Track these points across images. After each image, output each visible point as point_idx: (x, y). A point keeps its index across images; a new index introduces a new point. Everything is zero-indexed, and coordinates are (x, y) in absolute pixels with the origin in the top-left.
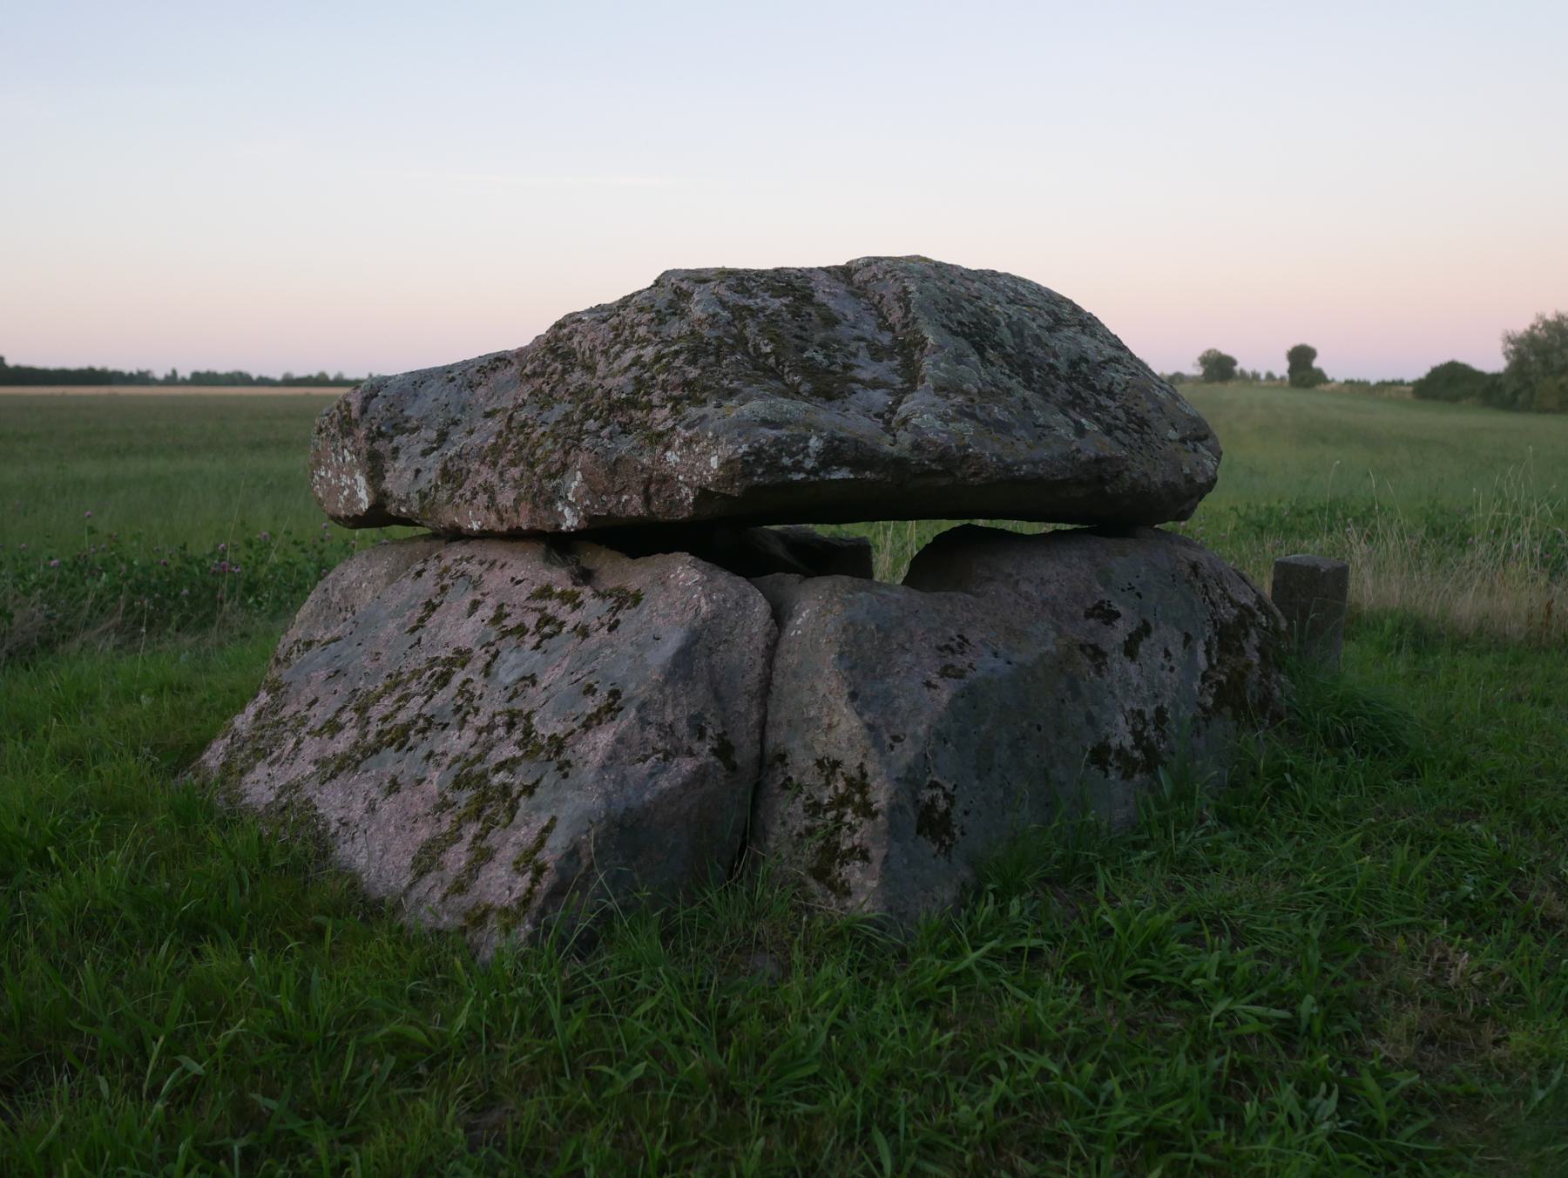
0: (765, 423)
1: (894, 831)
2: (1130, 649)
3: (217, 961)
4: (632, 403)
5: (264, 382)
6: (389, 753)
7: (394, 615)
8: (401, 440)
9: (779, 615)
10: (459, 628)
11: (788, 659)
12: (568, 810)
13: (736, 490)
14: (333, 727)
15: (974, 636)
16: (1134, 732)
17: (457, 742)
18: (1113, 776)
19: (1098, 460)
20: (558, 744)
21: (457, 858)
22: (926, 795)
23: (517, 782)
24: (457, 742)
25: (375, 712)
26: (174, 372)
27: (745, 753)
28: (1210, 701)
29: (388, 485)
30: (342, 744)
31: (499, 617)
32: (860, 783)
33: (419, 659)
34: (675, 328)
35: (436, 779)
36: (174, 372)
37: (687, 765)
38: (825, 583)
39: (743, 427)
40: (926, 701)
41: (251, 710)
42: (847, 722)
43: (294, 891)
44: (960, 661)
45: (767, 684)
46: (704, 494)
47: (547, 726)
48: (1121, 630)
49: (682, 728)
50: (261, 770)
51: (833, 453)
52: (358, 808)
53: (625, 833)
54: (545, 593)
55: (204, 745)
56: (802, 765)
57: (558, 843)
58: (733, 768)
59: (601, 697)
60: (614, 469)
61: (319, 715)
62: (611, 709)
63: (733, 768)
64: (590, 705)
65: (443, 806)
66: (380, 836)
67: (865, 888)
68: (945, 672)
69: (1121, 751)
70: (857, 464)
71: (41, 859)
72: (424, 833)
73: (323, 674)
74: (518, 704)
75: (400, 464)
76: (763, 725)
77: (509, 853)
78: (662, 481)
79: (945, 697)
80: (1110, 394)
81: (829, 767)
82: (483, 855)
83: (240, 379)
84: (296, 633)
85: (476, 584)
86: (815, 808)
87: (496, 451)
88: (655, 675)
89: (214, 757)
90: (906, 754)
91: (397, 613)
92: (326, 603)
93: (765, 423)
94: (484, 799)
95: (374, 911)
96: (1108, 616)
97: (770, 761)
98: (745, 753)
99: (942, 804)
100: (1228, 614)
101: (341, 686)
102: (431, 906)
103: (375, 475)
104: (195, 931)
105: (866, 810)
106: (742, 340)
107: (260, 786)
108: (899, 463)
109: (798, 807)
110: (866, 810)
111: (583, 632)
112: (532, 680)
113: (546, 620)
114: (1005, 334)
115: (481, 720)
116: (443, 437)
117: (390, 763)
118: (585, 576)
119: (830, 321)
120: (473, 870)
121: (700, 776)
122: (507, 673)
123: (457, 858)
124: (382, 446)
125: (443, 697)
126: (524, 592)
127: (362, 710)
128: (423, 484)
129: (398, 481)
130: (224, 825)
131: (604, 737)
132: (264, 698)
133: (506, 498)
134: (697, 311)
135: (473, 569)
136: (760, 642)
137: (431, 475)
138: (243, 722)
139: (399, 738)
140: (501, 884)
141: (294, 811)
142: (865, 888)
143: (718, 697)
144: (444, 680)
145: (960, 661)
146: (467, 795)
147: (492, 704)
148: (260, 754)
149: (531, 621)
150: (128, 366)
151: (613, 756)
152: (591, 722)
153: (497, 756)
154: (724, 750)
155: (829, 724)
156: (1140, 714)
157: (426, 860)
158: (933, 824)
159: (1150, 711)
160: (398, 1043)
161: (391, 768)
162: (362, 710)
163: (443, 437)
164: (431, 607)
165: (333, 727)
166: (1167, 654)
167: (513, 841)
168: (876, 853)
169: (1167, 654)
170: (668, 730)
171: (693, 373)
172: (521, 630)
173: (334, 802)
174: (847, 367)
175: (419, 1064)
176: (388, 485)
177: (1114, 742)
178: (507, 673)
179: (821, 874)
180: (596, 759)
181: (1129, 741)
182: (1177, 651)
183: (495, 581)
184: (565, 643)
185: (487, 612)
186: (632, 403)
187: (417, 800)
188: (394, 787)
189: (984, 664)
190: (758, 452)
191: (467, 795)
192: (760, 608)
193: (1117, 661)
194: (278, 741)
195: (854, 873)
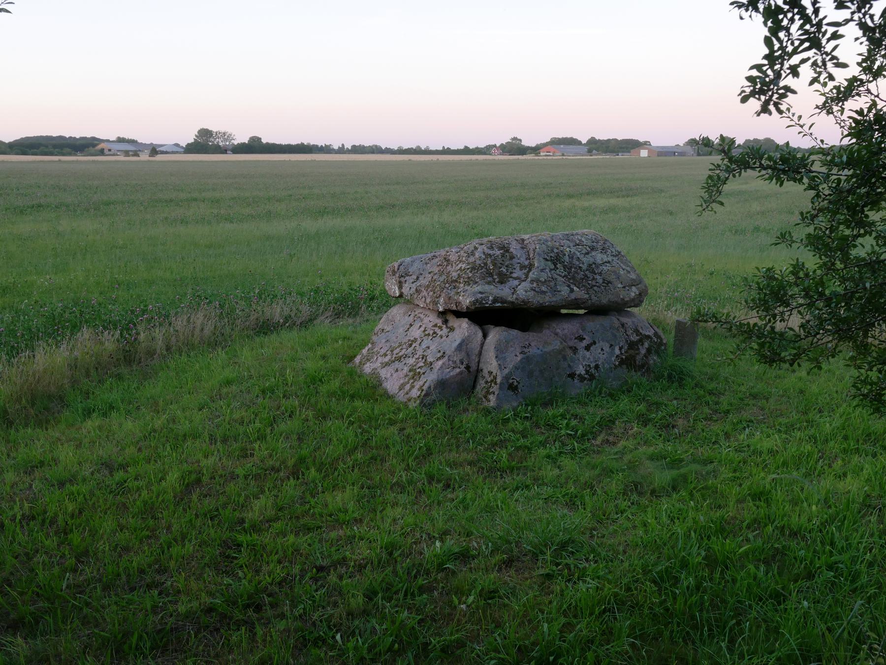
0: (480, 293)
1: (501, 388)
2: (587, 348)
3: (357, 403)
4: (456, 281)
5: (388, 151)
6: (397, 362)
7: (403, 326)
8: (407, 278)
9: (485, 336)
10: (416, 333)
11: (485, 347)
12: (430, 378)
13: (473, 308)
14: (385, 355)
15: (532, 344)
16: (586, 370)
17: (411, 361)
18: (576, 381)
19: (576, 299)
20: (431, 363)
21: (408, 387)
22: (511, 381)
23: (422, 371)
24: (411, 361)
25: (395, 352)
26: (343, 145)
27: (474, 367)
28: (617, 363)
29: (403, 290)
30: (387, 359)
31: (425, 331)
32: (495, 378)
33: (406, 340)
34: (472, 259)
35: (406, 369)
36: (343, 145)
37: (458, 370)
38: (498, 328)
39: (474, 294)
40: (514, 358)
41: (367, 348)
42: (494, 363)
43: (373, 390)
44: (526, 350)
45: (480, 353)
46: (467, 308)
47: (430, 359)
48: (585, 343)
49: (458, 362)
50: (368, 364)
51: (495, 300)
52: (389, 375)
53: (442, 384)
54: (435, 326)
55: (355, 357)
56: (485, 372)
57: (427, 385)
58: (469, 372)
59: (441, 354)
60: (450, 298)
61: (383, 351)
62: (443, 356)
63: (469, 372)
64: (439, 355)
65: (406, 376)
66: (392, 381)
67: (493, 400)
68: (521, 353)
69: (580, 375)
70: (502, 303)
71: (321, 380)
72: (402, 381)
73: (384, 341)
74: (425, 353)
75: (406, 285)
76: (479, 362)
77: (418, 387)
78: (458, 303)
79: (519, 359)
80: (600, 274)
81: (490, 373)
82: (412, 387)
83: (376, 150)
84: (380, 326)
85: (422, 320)
86: (487, 382)
87: (428, 286)
88: (453, 350)
89: (357, 360)
90: (506, 371)
91: (403, 326)
92: (388, 319)
93: (480, 293)
94: (415, 374)
95: (387, 396)
96: (581, 339)
97: (479, 371)
98: (474, 367)
99: (515, 384)
100: (634, 338)
101: (388, 344)
102: (401, 397)
103: (400, 287)
104: (352, 397)
105: (496, 383)
106: (486, 264)
107: (368, 368)
108: (513, 303)
109: (483, 382)
110: (496, 383)
111: (441, 337)
112: (428, 348)
113: (435, 333)
114: (567, 258)
115: (416, 356)
116: (418, 278)
117: (397, 365)
118: (446, 322)
119: (512, 258)
120: (410, 390)
121: (461, 373)
122: (424, 346)
123: (408, 387)
124: (402, 279)
125: (410, 349)
126: (432, 324)
127: (392, 351)
128: (411, 292)
129: (405, 290)
130: (359, 377)
131: (440, 363)
132: (370, 345)
133: (428, 300)
134: (477, 255)
135: (422, 316)
136: (479, 343)
137: (413, 290)
138: (365, 351)
139: (399, 359)
140: (415, 393)
141: (375, 373)
142: (493, 400)
143: (468, 355)
144: (410, 345)
145: (526, 350)
146: (411, 374)
147: (420, 353)
148: (368, 360)
149: (431, 332)
150: (320, 143)
151: (441, 367)
152: (439, 359)
153: (419, 365)
154: (468, 367)
155: (491, 364)
156: (589, 366)
157: (401, 388)
158: (513, 388)
159: (593, 365)
160: (390, 419)
161: (397, 366)
162: (392, 351)
163: (418, 278)
164: (411, 325)
165: (385, 355)
166: (602, 350)
167: (418, 384)
168: (496, 393)
169: (602, 350)
170: (455, 362)
171: (470, 275)
172: (429, 335)
173: (384, 373)
174: (511, 273)
175: (392, 423)
176: (403, 290)
177: (578, 373)
178: (424, 346)
179: (485, 397)
180: (438, 367)
181: (583, 372)
182: (607, 348)
183: (426, 320)
184: (437, 339)
185: (422, 329)
186: (456, 281)
187: (401, 374)
188: (397, 370)
189: (533, 351)
190: (477, 300)
191: (411, 374)
192: (480, 334)
193: (582, 352)
194: (372, 357)
195: (491, 397)
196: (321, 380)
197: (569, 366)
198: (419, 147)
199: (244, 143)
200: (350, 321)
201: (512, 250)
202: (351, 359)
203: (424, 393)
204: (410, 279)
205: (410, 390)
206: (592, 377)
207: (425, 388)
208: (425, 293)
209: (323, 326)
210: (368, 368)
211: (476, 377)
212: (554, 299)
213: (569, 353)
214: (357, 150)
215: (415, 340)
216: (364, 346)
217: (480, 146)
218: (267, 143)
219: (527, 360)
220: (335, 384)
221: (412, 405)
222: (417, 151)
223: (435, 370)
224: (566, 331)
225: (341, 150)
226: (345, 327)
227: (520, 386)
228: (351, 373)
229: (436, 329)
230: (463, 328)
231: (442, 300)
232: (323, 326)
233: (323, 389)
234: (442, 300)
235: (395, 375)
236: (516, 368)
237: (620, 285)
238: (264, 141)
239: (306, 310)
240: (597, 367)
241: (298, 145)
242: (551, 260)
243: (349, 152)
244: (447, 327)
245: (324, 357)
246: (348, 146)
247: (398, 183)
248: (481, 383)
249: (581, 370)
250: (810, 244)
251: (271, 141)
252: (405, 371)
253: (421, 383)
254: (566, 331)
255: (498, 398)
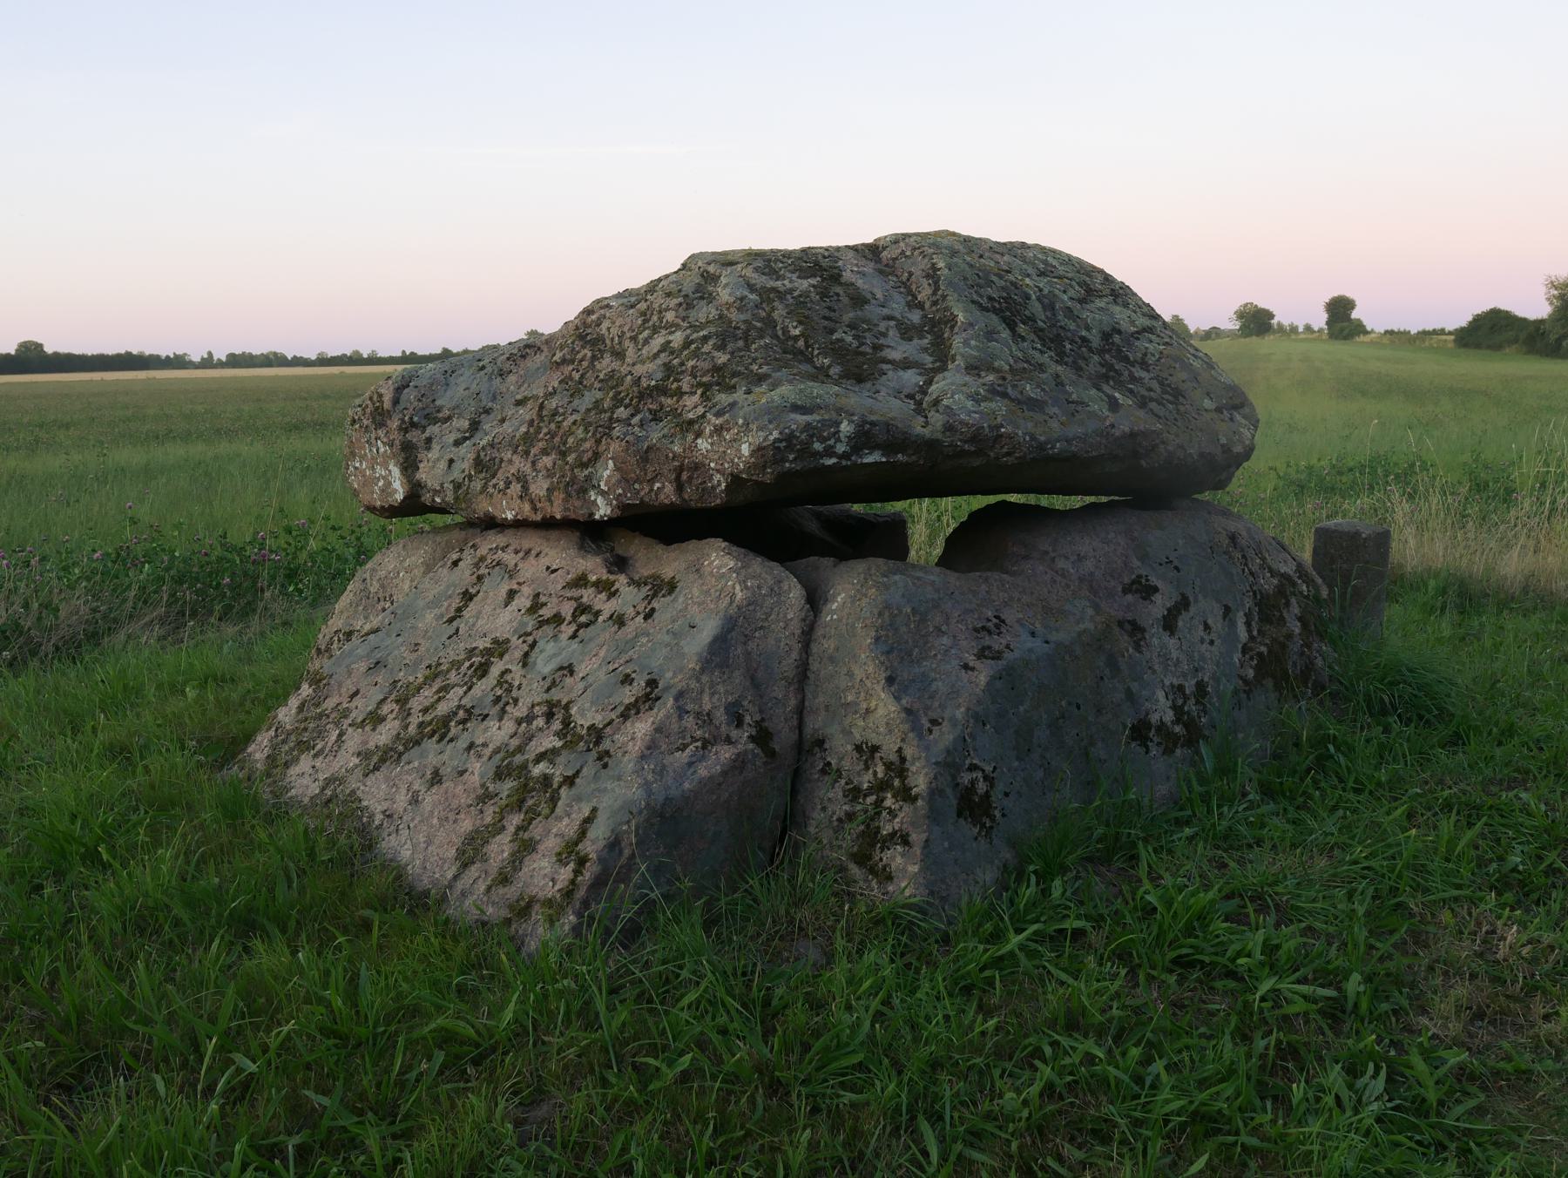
0: (796, 408)
1: (934, 816)
2: (1169, 623)
3: (267, 957)
5: (298, 362)
6: (431, 745)
8: (433, 430)
9: (815, 600)
10: (496, 618)
11: (825, 644)
12: (608, 801)
14: (375, 719)
15: (1010, 616)
17: (497, 733)
20: (597, 734)
21: (500, 849)
22: (966, 778)
23: (558, 772)
24: (497, 733)
25: (416, 704)
26: (210, 354)
27: (784, 737)
28: (1251, 673)
29: (422, 475)
30: (383, 736)
31: (535, 607)
32: (899, 768)
33: (457, 650)
34: (704, 312)
35: (478, 770)
36: (210, 354)
37: (726, 753)
38: (860, 566)
39: (773, 414)
40: (964, 682)
41: (294, 702)
42: (885, 707)
43: (343, 882)
44: (997, 643)
46: (735, 481)
47: (586, 716)
48: (1160, 604)
49: (720, 716)
50: (305, 763)
51: (864, 438)
52: (402, 799)
53: (665, 822)
55: (248, 738)
57: (599, 833)
58: (771, 754)
61: (361, 707)
63: (771, 754)
64: (628, 695)
65: (485, 797)
66: (422, 828)
67: (906, 873)
68: (982, 654)
69: (1161, 727)
70: (889, 447)
71: (91, 857)
72: (467, 825)
73: (362, 666)
74: (556, 695)
75: (434, 454)
76: (800, 711)
77: (551, 844)
78: (688, 471)
79: (983, 679)
80: (1144, 365)
81: (867, 751)
82: (525, 847)
84: (336, 623)
85: (512, 573)
86: (854, 793)
87: (528, 439)
89: (259, 749)
90: (944, 737)
93: (796, 408)
94: (525, 791)
95: (413, 902)
97: (809, 747)
98: (784, 737)
99: (982, 787)
100: (1268, 584)
101: (382, 677)
102: (476, 897)
104: (246, 927)
105: (906, 795)
106: (770, 323)
108: (931, 445)
109: (837, 792)
111: (619, 620)
112: (570, 669)
113: (582, 609)
114: (1036, 308)
115: (520, 711)
116: (475, 426)
117: (432, 754)
118: (620, 564)
120: (517, 860)
121: (739, 763)
122: (545, 663)
123: (500, 849)
124: (415, 436)
125: (483, 687)
126: (560, 580)
127: (402, 701)
128: (456, 474)
129: (432, 472)
130: (269, 819)
131: (641, 727)
132: (306, 690)
133: (539, 488)
134: (724, 295)
135: (509, 558)
136: (796, 628)
137: (465, 466)
138: (286, 714)
139: (440, 729)
140: (544, 875)
141: (336, 803)
142: (906, 873)
143: (755, 684)
144: (482, 671)
145: (997, 643)
146: (508, 785)
147: (531, 694)
148: (304, 746)
149: (567, 609)
151: (652, 746)
152: (630, 712)
154: (762, 737)
155: (868, 710)
156: (1181, 688)
157: (471, 851)
158: (973, 807)
159: (1190, 686)
160: (446, 1038)
161: (433, 760)
162: (402, 701)
163: (475, 426)
164: (468, 597)
165: (375, 719)
166: (1207, 627)
167: (556, 831)
168: (917, 837)
169: (1207, 627)
170: (706, 719)
171: (722, 358)
172: (557, 619)
173: (377, 794)
176: (422, 475)
177: (1154, 718)
178: (545, 663)
179: (862, 859)
180: (635, 748)
181: (1169, 716)
182: (1216, 622)
183: (531, 569)
184: (602, 632)
185: (523, 601)
187: (460, 792)
188: (436, 779)
189: (1021, 644)
190: (789, 439)
191: (508, 785)
192: (795, 593)
193: (1157, 638)
194: (321, 733)
195: (895, 858)
196: (91, 857)
197: (1130, 695)
198: (357, 352)
199: (8, 355)
200: (230, 630)
201: (847, 276)
202: (235, 745)
203: (588, 875)
204: (443, 435)
205: (517, 860)
206: (1193, 733)
207: (590, 848)
208: (519, 464)
209: (139, 651)
210: (304, 779)
211: (797, 774)
212: (1075, 430)
213: (1124, 641)
214: (235, 361)
215: (500, 647)
216: (282, 699)
217: (471, 348)
218: (56, 354)
219: (1009, 681)
220: (157, 872)
221: (538, 933)
222: (355, 360)
223: (628, 764)
224: (1089, 565)
225: (208, 363)
226: (216, 646)
227: (996, 795)
228: (235, 809)
229: (587, 595)
230: (715, 575)
231: (606, 472)
232: (139, 651)
233: (104, 897)
234: (606, 472)
235: (429, 799)
236: (980, 720)
237: (1207, 404)
238: (49, 349)
239: (75, 608)
240: (1201, 687)
241: (119, 355)
242: (995, 311)
243: (221, 365)
244: (633, 582)
245: (120, 754)
246: (220, 355)
247: (326, 397)
248: (828, 802)
249: (1161, 710)
250: (1466, 345)
251: (64, 349)
252: (474, 779)
253: (566, 826)
254: (1089, 565)
255: (931, 861)
